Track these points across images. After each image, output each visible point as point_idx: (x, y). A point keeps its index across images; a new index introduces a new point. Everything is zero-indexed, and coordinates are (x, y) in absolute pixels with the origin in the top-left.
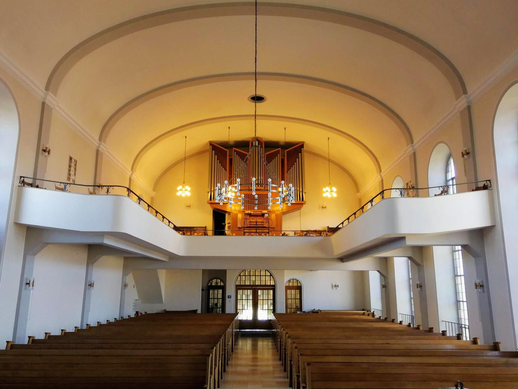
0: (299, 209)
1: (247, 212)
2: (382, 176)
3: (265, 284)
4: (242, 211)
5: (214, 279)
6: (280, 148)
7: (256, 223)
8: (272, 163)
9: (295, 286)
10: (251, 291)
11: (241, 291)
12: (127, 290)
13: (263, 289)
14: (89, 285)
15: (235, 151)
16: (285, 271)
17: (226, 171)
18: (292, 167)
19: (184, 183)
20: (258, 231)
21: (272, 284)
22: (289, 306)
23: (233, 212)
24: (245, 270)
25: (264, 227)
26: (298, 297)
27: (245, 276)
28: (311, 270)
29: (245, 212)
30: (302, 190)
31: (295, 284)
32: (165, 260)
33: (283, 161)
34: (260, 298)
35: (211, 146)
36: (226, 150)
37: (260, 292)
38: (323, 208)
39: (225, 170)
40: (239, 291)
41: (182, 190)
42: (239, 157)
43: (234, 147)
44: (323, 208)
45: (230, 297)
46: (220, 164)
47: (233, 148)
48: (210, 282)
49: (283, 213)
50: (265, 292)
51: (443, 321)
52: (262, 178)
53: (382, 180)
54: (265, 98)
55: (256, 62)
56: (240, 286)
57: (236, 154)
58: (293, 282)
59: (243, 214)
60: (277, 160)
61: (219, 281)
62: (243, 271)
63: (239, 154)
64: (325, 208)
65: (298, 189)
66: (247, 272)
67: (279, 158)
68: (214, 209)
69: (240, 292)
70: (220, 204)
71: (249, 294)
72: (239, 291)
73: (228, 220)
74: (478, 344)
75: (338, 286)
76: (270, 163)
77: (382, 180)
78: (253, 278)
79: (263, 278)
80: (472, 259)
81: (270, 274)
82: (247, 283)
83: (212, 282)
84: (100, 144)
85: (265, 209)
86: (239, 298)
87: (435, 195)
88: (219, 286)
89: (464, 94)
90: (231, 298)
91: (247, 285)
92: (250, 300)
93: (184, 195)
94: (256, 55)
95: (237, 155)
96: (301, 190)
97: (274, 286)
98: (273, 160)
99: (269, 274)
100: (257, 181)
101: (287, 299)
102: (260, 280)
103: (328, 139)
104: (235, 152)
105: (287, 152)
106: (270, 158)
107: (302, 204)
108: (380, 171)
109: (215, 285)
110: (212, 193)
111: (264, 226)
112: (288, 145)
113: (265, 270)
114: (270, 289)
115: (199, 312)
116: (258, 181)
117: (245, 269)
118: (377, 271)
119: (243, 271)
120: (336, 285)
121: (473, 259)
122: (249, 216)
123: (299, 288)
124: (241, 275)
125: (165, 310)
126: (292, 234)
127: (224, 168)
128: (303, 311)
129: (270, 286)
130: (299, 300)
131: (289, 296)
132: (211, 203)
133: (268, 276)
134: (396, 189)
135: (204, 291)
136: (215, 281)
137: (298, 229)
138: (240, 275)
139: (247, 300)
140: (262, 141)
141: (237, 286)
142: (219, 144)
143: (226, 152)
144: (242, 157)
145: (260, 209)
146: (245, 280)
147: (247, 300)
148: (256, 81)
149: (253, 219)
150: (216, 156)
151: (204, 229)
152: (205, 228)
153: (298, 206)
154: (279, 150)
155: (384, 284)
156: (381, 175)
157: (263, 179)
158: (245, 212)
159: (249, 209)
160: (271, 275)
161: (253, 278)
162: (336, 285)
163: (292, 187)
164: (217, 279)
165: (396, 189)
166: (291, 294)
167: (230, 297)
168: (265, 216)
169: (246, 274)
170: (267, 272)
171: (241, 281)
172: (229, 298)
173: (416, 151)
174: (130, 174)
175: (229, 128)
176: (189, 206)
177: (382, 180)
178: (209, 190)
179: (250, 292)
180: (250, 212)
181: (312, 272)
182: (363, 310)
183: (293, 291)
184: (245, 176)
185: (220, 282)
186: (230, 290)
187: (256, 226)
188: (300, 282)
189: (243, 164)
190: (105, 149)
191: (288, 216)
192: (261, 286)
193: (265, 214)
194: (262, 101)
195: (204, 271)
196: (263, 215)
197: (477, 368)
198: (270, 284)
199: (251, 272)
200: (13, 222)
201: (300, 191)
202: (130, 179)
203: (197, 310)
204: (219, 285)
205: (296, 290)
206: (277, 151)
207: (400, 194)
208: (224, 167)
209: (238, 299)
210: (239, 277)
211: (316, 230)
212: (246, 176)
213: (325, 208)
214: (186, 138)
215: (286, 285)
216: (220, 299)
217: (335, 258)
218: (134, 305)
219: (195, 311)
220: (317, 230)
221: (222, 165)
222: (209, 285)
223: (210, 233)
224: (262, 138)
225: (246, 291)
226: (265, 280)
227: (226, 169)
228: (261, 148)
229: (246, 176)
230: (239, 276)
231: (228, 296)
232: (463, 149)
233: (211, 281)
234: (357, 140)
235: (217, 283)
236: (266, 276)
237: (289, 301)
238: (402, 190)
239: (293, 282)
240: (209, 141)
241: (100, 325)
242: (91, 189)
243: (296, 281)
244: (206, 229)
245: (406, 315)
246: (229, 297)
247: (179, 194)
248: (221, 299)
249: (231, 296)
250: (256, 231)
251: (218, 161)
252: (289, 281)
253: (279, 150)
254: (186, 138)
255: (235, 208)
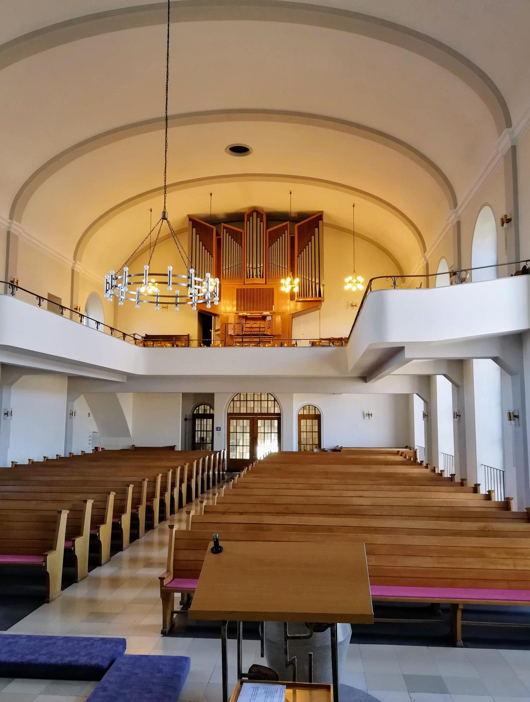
0: (318, 308)
1: (241, 314)
2: (427, 258)
3: (247, 412)
4: (236, 313)
5: (202, 405)
6: (288, 222)
7: (259, 329)
8: (275, 245)
9: (312, 415)
10: (249, 421)
11: (235, 421)
12: (75, 420)
13: (264, 419)
14: (5, 414)
15: (225, 228)
16: (294, 395)
17: (212, 256)
18: (306, 248)
19: (354, 271)
20: (244, 340)
21: (276, 412)
22: (303, 441)
23: (222, 313)
24: (240, 394)
25: (265, 334)
26: (316, 429)
27: (240, 401)
28: (334, 394)
29: (238, 313)
30: (318, 282)
31: (312, 412)
32: (121, 381)
33: (292, 239)
34: (261, 430)
35: (191, 222)
36: (212, 226)
37: (260, 423)
38: (353, 306)
40: (231, 421)
41: (352, 282)
42: (230, 236)
43: (224, 223)
44: (353, 306)
45: (219, 429)
46: (204, 247)
47: (222, 223)
48: (195, 409)
49: (292, 314)
50: (268, 422)
51: (482, 465)
52: (262, 265)
53: (427, 264)
54: (250, 149)
55: (167, 93)
56: (233, 414)
57: (226, 233)
58: (309, 410)
59: (237, 317)
60: (285, 239)
61: (208, 407)
62: (238, 394)
63: (229, 231)
64: (355, 306)
66: (242, 396)
67: (286, 237)
68: (199, 311)
69: (233, 422)
70: (215, 303)
71: (245, 425)
72: (231, 421)
73: (217, 324)
74: (491, 500)
75: (371, 415)
77: (426, 264)
78: (251, 404)
79: (265, 404)
80: (509, 377)
81: (274, 398)
82: (243, 411)
83: (199, 409)
84: (11, 224)
85: (266, 310)
86: (231, 430)
87: (417, 288)
88: (208, 414)
89: (507, 127)
90: (220, 430)
91: (242, 413)
92: (247, 433)
93: (354, 289)
94: (167, 81)
96: (317, 281)
97: (279, 414)
98: (278, 239)
99: (273, 399)
100: (255, 270)
101: (301, 432)
102: (261, 407)
103: (354, 206)
104: (225, 230)
105: (298, 227)
106: (273, 237)
107: (320, 301)
108: (425, 250)
109: (203, 413)
111: (265, 333)
112: (302, 216)
113: (268, 394)
114: (274, 419)
115: (179, 448)
116: (226, 271)
117: (240, 392)
118: (416, 394)
119: (238, 394)
120: (368, 412)
121: (510, 377)
123: (318, 417)
124: (235, 400)
125: (133, 445)
126: (307, 344)
127: (208, 253)
128: (322, 448)
129: (274, 414)
130: (317, 433)
131: (303, 429)
133: (271, 401)
134: (387, 277)
135: (187, 421)
136: (203, 408)
137: (316, 336)
138: (233, 400)
139: (243, 433)
140: (263, 213)
141: (229, 414)
142: (201, 219)
143: (212, 229)
144: (237, 237)
146: (240, 407)
147: (243, 433)
148: (167, 122)
149: (255, 323)
150: (198, 236)
151: (186, 338)
152: (187, 337)
153: (315, 304)
154: (287, 225)
155: (456, 411)
156: (425, 257)
157: (263, 267)
158: (238, 313)
159: (244, 310)
160: (275, 400)
161: (251, 404)
162: (368, 412)
163: (209, 279)
164: (205, 406)
165: (387, 277)
166: (306, 426)
167: (219, 429)
168: (267, 319)
169: (242, 399)
170: (269, 396)
171: (234, 408)
172: (217, 430)
173: (461, 219)
174: (72, 265)
175: (211, 195)
176: (166, 307)
177: (427, 264)
179: (247, 423)
180: (245, 314)
181: (335, 396)
182: (406, 447)
183: (309, 422)
185: (210, 409)
186: (221, 420)
187: (259, 333)
188: (318, 410)
189: (235, 245)
190: (21, 231)
191: (302, 318)
192: (261, 414)
193: (267, 317)
194: (245, 153)
195: (185, 395)
196: (264, 318)
197: (415, 536)
198: (273, 412)
199: (248, 395)
202: (73, 271)
203: (175, 446)
204: (209, 413)
205: (313, 420)
206: (284, 226)
207: (393, 285)
208: (209, 252)
209: (258, 433)
210: (232, 402)
211: (342, 338)
213: (355, 306)
214: (151, 211)
215: (300, 413)
216: (209, 431)
217: (355, 377)
218: (91, 438)
219: (172, 448)
220: (343, 337)
221: (206, 248)
222: (195, 412)
223: (195, 343)
224: (262, 209)
225: (241, 421)
226: (268, 407)
228: (260, 222)
229: (240, 263)
230: (232, 401)
231: (217, 428)
232: (503, 213)
233: (197, 408)
234: (389, 205)
235: (205, 410)
236: (269, 402)
237: (304, 435)
238: (396, 278)
239: (309, 410)
241: (16, 465)
242: (423, 279)
243: (314, 407)
244: (188, 338)
245: (448, 456)
246: (218, 430)
247: (347, 287)
248: (211, 431)
249: (220, 428)
250: (242, 340)
251: (201, 242)
252: (303, 407)
254: (151, 211)
255: (225, 309)
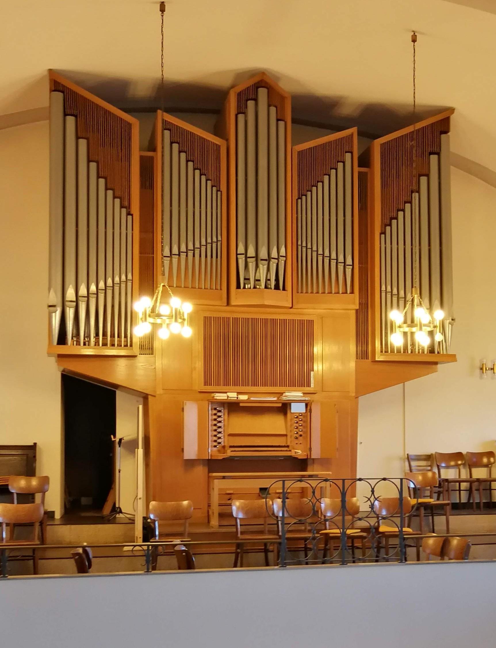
6: (354, 130)
15: (167, 126)
18: (403, 210)
35: (60, 96)
39: (124, 211)
43: (168, 110)
47: (159, 112)
65: (395, 291)
76: (314, 189)
85: (293, 384)
95: (175, 146)
98: (326, 178)
110: (68, 309)
122: (226, 411)
132: (61, 356)
142: (92, 90)
145: (274, 384)
150: (83, 143)
178: (54, 298)
180: (233, 396)
184: (209, 240)
200: (218, 493)
201: (393, 293)
212: (215, 239)
221: (109, 186)
227: (126, 206)
240: (51, 71)
253: (352, 135)
